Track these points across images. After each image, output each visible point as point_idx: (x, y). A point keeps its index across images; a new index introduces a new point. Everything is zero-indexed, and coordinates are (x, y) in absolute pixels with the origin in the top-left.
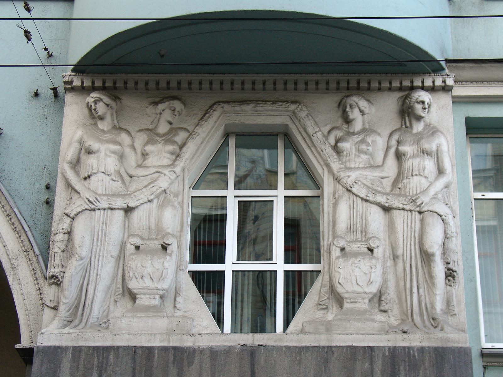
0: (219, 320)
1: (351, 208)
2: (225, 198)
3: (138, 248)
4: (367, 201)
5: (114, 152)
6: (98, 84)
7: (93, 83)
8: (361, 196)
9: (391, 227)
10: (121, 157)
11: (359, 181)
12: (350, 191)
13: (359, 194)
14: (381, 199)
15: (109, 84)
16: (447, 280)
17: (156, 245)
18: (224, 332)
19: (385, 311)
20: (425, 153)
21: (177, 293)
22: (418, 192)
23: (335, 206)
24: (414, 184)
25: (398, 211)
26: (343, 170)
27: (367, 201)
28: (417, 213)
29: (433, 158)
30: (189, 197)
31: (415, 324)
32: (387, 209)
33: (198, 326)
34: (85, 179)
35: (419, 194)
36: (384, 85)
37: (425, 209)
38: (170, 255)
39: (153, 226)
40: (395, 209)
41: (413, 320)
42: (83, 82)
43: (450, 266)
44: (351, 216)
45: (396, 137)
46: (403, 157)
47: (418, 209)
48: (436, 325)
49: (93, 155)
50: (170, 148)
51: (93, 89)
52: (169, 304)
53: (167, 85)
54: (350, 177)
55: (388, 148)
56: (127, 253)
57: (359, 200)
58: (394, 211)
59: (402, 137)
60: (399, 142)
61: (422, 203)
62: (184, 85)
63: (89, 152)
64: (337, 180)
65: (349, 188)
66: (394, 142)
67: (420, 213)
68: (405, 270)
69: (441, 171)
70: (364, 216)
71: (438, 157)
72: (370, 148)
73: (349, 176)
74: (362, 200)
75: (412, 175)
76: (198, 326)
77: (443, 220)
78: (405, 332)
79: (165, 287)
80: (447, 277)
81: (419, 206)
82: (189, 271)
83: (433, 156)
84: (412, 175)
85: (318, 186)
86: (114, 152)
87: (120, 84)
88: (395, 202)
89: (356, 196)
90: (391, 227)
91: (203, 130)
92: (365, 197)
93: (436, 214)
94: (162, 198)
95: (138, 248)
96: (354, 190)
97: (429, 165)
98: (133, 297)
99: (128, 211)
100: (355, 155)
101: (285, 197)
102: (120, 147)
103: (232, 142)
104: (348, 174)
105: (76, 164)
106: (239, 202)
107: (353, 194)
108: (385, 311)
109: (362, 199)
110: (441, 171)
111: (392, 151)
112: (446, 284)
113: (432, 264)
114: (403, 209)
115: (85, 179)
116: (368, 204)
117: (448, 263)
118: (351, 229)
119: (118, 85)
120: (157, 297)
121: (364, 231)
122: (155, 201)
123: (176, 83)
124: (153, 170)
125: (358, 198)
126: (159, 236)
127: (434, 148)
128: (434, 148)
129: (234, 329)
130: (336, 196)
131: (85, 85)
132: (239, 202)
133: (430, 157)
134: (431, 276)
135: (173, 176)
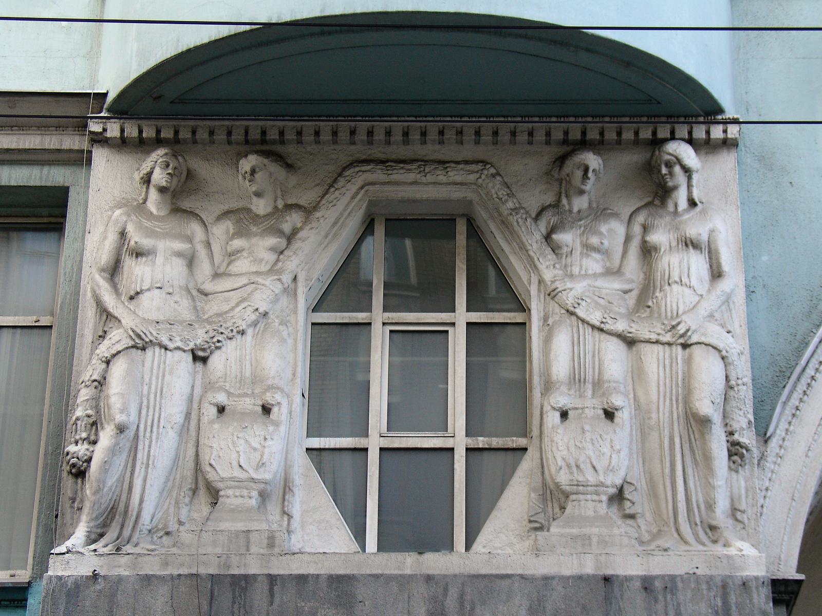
0: (360, 534)
1: (575, 343)
2: (364, 329)
3: (221, 410)
4: (601, 330)
5: (179, 254)
6: (149, 133)
7: (158, 132)
8: (591, 323)
9: (637, 373)
10: (191, 261)
11: (586, 296)
12: (572, 314)
13: (588, 319)
14: (620, 326)
15: (167, 134)
16: (732, 463)
17: (250, 404)
18: (367, 551)
19: (632, 517)
20: (691, 244)
21: (287, 488)
22: (680, 312)
23: (547, 340)
24: (675, 298)
25: (648, 346)
26: (560, 278)
27: (601, 330)
28: (679, 348)
29: (703, 252)
30: (306, 324)
31: (682, 538)
32: (631, 342)
33: (319, 537)
34: (132, 298)
35: (684, 313)
36: (377, 138)
37: (694, 339)
38: (277, 424)
39: (248, 373)
40: (642, 341)
41: (677, 530)
42: (141, 132)
43: (736, 437)
44: (576, 358)
45: (641, 218)
46: (653, 254)
47: (681, 341)
48: (715, 538)
49: (144, 259)
50: (272, 241)
51: (159, 142)
52: (273, 508)
53: (262, 136)
54: (573, 291)
55: (628, 239)
56: (205, 420)
57: (589, 330)
58: (643, 345)
59: (650, 220)
60: (645, 229)
61: (688, 330)
62: (290, 136)
63: (138, 254)
64: (552, 295)
65: (572, 309)
66: (637, 229)
67: (685, 346)
68: (661, 447)
69: (716, 274)
70: (597, 353)
71: (709, 252)
72: (606, 242)
73: (571, 289)
74: (592, 329)
75: (669, 284)
76: (319, 537)
77: (723, 358)
78: (665, 550)
79: (267, 476)
80: (731, 455)
81: (682, 336)
82: (307, 449)
83: (703, 250)
84: (669, 284)
85: (523, 308)
86: (179, 254)
87: (185, 134)
88: (641, 330)
89: (583, 321)
90: (637, 373)
91: (327, 215)
92: (597, 324)
93: (711, 348)
94: (261, 326)
95: (221, 410)
96: (580, 312)
97: (698, 264)
98: (214, 495)
99: (199, 343)
100: (581, 253)
101: (468, 324)
102: (190, 246)
103: (380, 230)
104: (569, 285)
105: (114, 270)
106: (391, 331)
107: (578, 318)
108: (632, 517)
109: (593, 327)
110: (716, 274)
111: (635, 244)
112: (729, 467)
113: (707, 437)
114: (657, 342)
115: (132, 298)
116: (603, 336)
117: (732, 433)
118: (576, 380)
119: (181, 136)
120: (255, 494)
121: (598, 384)
122: (250, 332)
123: (277, 132)
124: (244, 280)
125: (586, 325)
126: (258, 391)
127: (704, 238)
128: (704, 238)
129: (383, 546)
130: (550, 322)
131: (144, 135)
132: (391, 331)
133: (699, 252)
134: (708, 458)
135: (278, 288)
